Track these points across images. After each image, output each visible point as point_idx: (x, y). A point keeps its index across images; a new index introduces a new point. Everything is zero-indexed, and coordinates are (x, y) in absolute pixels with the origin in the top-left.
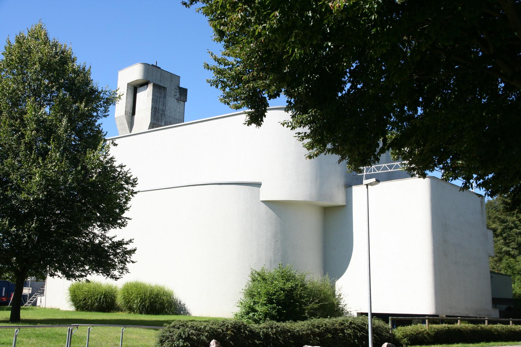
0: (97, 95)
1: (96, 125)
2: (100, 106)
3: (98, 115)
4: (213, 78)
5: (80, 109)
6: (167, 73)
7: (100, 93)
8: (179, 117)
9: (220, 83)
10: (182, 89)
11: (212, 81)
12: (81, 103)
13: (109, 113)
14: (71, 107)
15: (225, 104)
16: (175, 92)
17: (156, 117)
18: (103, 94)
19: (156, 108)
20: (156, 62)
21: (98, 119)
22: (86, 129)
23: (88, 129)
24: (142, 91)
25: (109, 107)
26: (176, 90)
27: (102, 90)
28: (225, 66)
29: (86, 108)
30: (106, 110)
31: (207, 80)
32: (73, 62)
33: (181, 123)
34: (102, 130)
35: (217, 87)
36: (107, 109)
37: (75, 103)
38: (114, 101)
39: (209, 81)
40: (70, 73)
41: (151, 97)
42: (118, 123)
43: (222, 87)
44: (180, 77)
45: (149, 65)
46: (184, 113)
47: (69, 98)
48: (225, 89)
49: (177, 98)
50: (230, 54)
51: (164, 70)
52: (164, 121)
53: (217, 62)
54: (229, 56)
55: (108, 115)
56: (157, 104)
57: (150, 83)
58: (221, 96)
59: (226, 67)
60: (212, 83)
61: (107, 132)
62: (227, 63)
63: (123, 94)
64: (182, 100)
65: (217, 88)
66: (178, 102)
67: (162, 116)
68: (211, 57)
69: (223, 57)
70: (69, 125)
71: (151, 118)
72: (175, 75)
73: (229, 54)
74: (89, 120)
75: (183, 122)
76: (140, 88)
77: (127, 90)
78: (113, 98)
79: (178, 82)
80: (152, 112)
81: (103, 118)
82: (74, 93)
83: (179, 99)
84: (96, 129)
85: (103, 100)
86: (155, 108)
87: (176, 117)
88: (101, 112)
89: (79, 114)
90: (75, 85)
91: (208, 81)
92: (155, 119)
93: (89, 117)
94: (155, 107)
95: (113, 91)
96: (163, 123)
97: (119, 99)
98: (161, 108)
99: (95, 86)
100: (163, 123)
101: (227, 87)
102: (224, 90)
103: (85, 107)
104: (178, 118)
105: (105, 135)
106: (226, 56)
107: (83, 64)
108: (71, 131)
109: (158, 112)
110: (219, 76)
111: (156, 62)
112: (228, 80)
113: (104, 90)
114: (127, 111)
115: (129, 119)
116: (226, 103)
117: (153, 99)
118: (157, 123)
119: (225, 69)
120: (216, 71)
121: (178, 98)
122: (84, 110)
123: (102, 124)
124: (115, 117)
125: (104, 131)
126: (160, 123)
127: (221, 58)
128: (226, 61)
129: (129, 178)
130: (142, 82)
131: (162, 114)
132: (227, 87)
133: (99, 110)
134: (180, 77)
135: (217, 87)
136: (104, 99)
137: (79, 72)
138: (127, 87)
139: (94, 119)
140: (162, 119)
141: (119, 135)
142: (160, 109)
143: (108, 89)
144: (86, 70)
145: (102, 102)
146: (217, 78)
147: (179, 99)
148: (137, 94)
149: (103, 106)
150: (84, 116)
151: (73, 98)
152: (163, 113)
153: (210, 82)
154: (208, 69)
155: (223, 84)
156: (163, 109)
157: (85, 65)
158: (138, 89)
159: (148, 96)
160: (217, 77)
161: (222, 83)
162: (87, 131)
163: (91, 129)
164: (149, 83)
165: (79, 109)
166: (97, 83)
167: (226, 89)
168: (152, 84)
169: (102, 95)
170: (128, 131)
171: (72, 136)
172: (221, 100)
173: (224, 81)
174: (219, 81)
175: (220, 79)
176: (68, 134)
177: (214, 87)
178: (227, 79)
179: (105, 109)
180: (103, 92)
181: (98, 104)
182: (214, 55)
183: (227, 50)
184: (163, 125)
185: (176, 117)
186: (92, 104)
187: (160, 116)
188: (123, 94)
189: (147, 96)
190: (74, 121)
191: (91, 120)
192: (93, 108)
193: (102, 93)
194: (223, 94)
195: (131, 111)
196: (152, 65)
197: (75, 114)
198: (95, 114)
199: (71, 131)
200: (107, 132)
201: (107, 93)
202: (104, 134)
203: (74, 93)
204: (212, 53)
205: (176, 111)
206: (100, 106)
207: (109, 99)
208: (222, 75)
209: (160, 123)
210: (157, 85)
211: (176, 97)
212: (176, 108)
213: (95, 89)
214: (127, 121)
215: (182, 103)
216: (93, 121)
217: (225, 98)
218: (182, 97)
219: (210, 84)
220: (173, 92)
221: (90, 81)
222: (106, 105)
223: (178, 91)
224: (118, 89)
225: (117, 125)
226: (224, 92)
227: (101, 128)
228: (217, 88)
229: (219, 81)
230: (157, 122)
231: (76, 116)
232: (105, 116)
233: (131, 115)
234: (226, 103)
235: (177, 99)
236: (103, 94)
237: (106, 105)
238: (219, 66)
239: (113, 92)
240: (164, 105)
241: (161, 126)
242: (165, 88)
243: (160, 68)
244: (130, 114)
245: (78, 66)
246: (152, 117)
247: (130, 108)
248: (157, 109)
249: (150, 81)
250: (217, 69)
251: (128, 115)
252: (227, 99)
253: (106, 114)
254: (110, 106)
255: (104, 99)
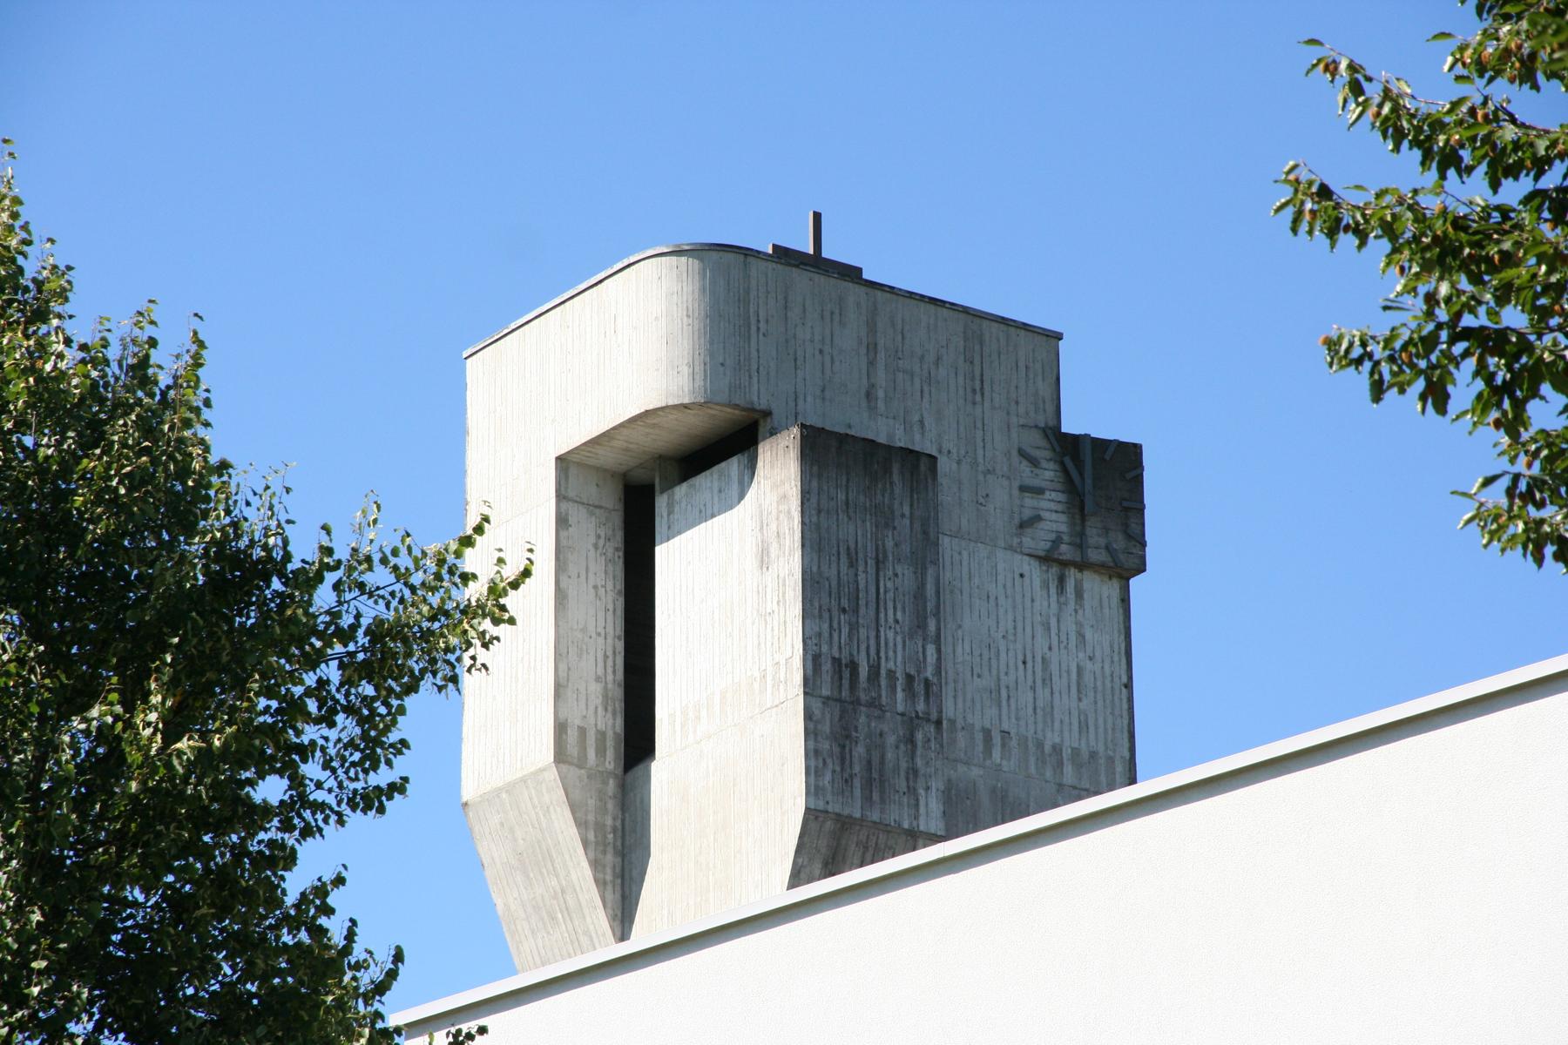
0: (282, 608)
1: (290, 900)
2: (312, 706)
3: (302, 797)
4: (1394, 318)
5: (134, 757)
6: (925, 313)
7: (308, 580)
8: (1083, 727)
9: (1466, 354)
10: (1133, 474)
11: (1378, 351)
12: (134, 696)
13: (403, 765)
14: (47, 748)
15: (1539, 560)
16: (1023, 489)
17: (860, 750)
18: (337, 587)
19: (853, 666)
20: (817, 217)
21: (307, 832)
22: (203, 946)
23: (218, 947)
24: (706, 515)
25: (402, 710)
26: (1025, 467)
27: (328, 551)
28: (1495, 186)
29: (183, 744)
30: (377, 742)
31: (1331, 344)
32: (41, 315)
33: (1111, 787)
34: (350, 936)
35: (1437, 396)
36: (387, 729)
37: (77, 700)
38: (448, 650)
39: (1357, 352)
40: (21, 425)
41: (789, 564)
42: (493, 851)
43: (1494, 394)
44: (1058, 337)
45: (747, 253)
46: (1129, 686)
47: (21, 661)
48: (1519, 406)
49: (1042, 546)
50: (1544, 55)
51: (892, 290)
52: (937, 784)
53: (1417, 154)
54: (1527, 76)
55: (397, 788)
56: (854, 627)
57: (773, 432)
58: (1488, 481)
59: (1513, 191)
60: (1385, 368)
61: (398, 957)
62: (1517, 146)
63: (526, 573)
64: (1095, 556)
65: (1441, 409)
66: (1061, 580)
67: (919, 736)
68: (1354, 110)
69: (1474, 92)
70: (37, 917)
71: (813, 772)
72: (1004, 321)
73: (1533, 56)
74: (221, 858)
75: (1132, 780)
76: (681, 490)
77: (562, 521)
78: (433, 618)
79: (1045, 390)
80: (817, 705)
81: (355, 819)
82: (70, 610)
83: (1066, 551)
84: (287, 939)
85: (338, 648)
86: (845, 669)
87: (1051, 739)
88: (326, 765)
89: (122, 806)
90: (73, 535)
91: (1342, 355)
92: (848, 781)
93: (221, 828)
94: (836, 662)
95: (431, 548)
96: (931, 813)
97: (497, 622)
98: (895, 661)
99: (255, 519)
100: (931, 813)
101: (1546, 388)
102: (1513, 425)
103: (172, 730)
104: (1071, 740)
105: (381, 988)
106: (1502, 82)
107: (126, 322)
108: (60, 986)
109: (874, 704)
110: (1444, 289)
111: (817, 217)
112: (1544, 313)
113: (342, 553)
114: (575, 721)
115: (601, 798)
116: (1550, 550)
117: (812, 584)
118: (875, 817)
119: (1505, 212)
120: (1416, 239)
121: (1057, 542)
122: (169, 766)
123: (339, 881)
124: (468, 793)
125: (373, 944)
126: (897, 814)
127: (1455, 105)
128: (1509, 133)
129: (469, 606)
130: (697, 425)
131: (911, 722)
132: (1546, 388)
133: (305, 752)
134: (1058, 337)
135: (1437, 396)
136: (346, 636)
137: (102, 401)
138: (560, 497)
139: (271, 843)
140: (913, 772)
141: (514, 972)
142: (891, 674)
143: (378, 539)
144: (164, 380)
145: (332, 672)
146: (1430, 314)
147: (1066, 551)
148: (661, 552)
149: (349, 710)
150: (168, 816)
151: (55, 659)
152: (921, 707)
153: (1358, 362)
154: (1332, 233)
155: (1492, 361)
156: (921, 664)
157: (150, 331)
158: (661, 503)
159: (764, 561)
160: (1431, 299)
161: (1487, 351)
162: (207, 969)
163: (244, 945)
164: (762, 430)
165: (122, 758)
166: (276, 487)
167: (1533, 408)
168: (795, 431)
169: (324, 597)
170: (599, 920)
171: (72, 1027)
172: (1492, 524)
173: (1503, 334)
174: (1452, 341)
175: (1458, 316)
176: (33, 1016)
177: (1406, 404)
178: (1535, 309)
179: (365, 736)
180: (339, 574)
181: (298, 690)
182: (1373, 91)
183: (1507, 18)
184: (935, 825)
185: (1051, 739)
186: (243, 693)
187: (891, 740)
188: (526, 573)
189: (751, 562)
190: (84, 883)
191: (240, 852)
192: (249, 731)
193: (330, 578)
194: (1503, 464)
195: (611, 723)
196: (783, 254)
197: (83, 816)
198: (272, 790)
199: (60, 986)
200: (398, 957)
201: (380, 577)
202: (366, 979)
203: (70, 610)
204: (1353, 68)
205: (1047, 680)
206: (312, 706)
207: (398, 631)
208: (1476, 279)
209: (897, 814)
210: (843, 439)
211: (1039, 539)
212: (1041, 643)
213: (258, 553)
214: (581, 824)
215: (1098, 588)
216: (261, 861)
217: (1528, 497)
218: (1094, 536)
219: (1359, 380)
220: (1001, 495)
221: (203, 484)
222: (369, 690)
223: (1048, 473)
224: (479, 530)
225: (488, 873)
226: (1514, 435)
227: (335, 928)
228: (1441, 409)
229: (1452, 341)
230: (868, 799)
231: (97, 829)
232: (372, 801)
233: (612, 760)
234: (1550, 550)
235: (1046, 559)
236: (337, 587)
237: (369, 690)
238: (1439, 189)
239: (430, 564)
240: (921, 625)
241: (915, 839)
242: (923, 466)
243: (851, 273)
244: (601, 751)
245: (84, 347)
246: (813, 754)
247: (595, 689)
248: (863, 671)
249: (767, 414)
250: (1420, 217)
251: (581, 764)
252: (1549, 512)
253: (382, 777)
254: (410, 701)
255: (346, 636)
